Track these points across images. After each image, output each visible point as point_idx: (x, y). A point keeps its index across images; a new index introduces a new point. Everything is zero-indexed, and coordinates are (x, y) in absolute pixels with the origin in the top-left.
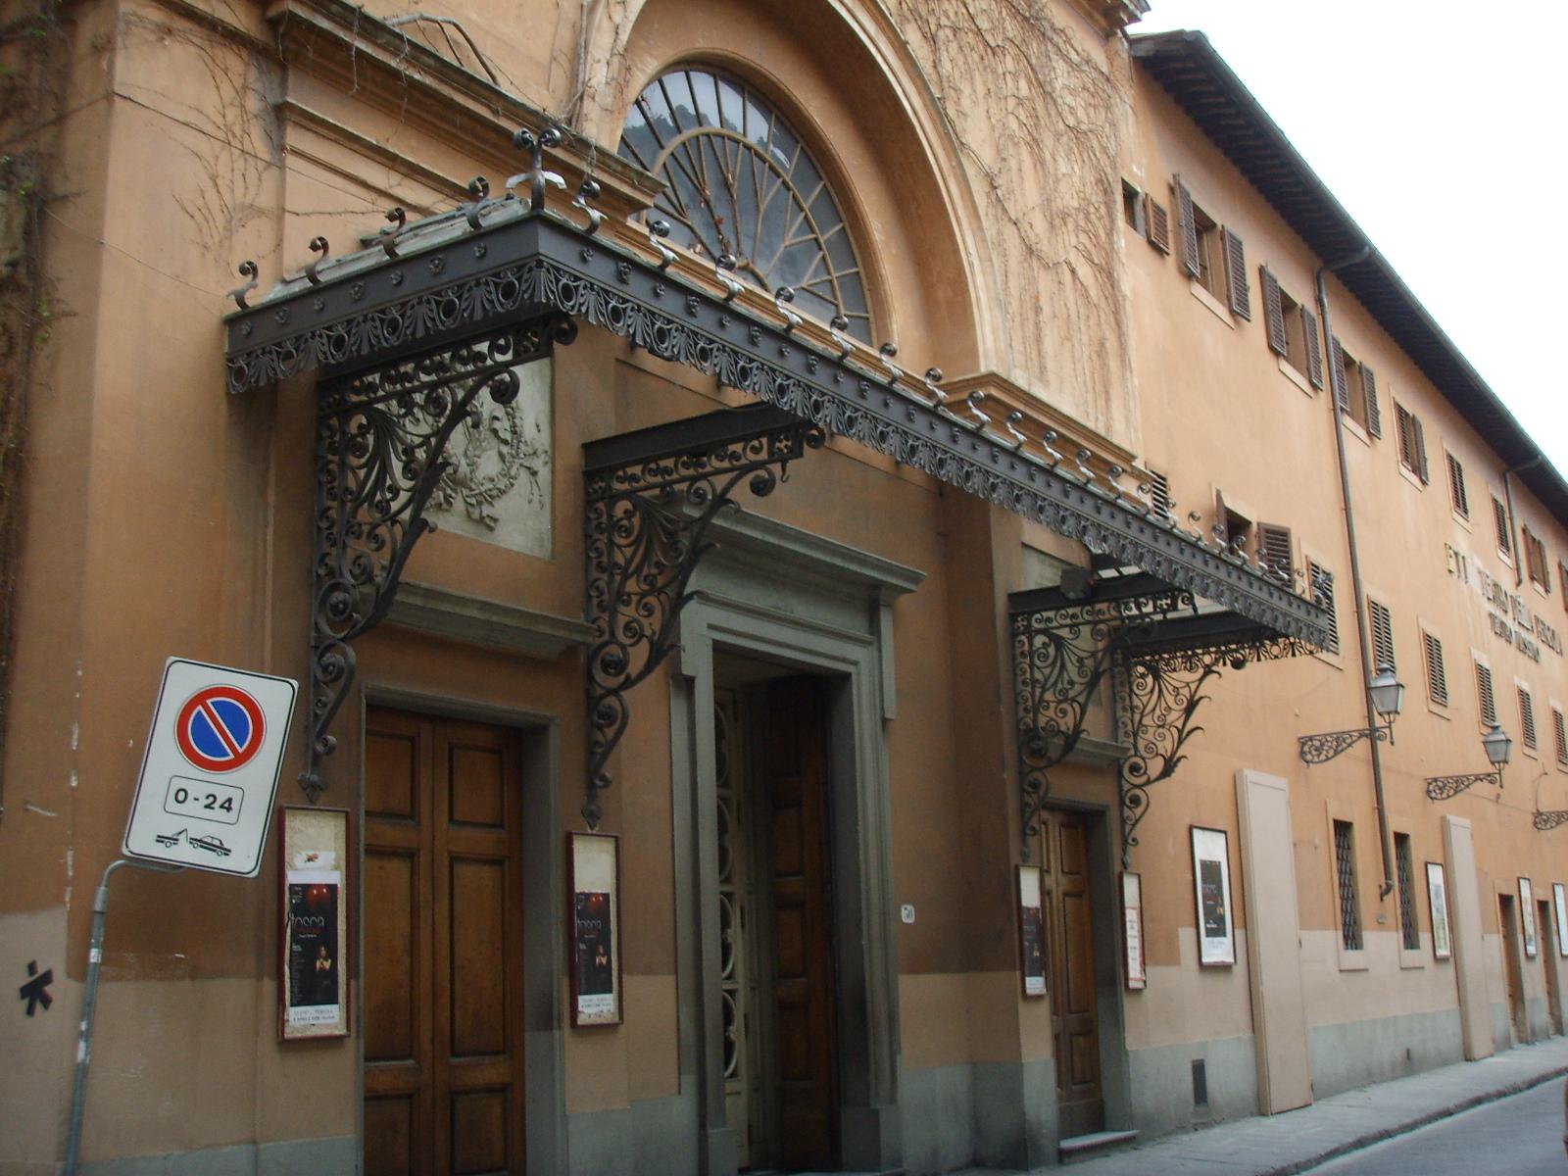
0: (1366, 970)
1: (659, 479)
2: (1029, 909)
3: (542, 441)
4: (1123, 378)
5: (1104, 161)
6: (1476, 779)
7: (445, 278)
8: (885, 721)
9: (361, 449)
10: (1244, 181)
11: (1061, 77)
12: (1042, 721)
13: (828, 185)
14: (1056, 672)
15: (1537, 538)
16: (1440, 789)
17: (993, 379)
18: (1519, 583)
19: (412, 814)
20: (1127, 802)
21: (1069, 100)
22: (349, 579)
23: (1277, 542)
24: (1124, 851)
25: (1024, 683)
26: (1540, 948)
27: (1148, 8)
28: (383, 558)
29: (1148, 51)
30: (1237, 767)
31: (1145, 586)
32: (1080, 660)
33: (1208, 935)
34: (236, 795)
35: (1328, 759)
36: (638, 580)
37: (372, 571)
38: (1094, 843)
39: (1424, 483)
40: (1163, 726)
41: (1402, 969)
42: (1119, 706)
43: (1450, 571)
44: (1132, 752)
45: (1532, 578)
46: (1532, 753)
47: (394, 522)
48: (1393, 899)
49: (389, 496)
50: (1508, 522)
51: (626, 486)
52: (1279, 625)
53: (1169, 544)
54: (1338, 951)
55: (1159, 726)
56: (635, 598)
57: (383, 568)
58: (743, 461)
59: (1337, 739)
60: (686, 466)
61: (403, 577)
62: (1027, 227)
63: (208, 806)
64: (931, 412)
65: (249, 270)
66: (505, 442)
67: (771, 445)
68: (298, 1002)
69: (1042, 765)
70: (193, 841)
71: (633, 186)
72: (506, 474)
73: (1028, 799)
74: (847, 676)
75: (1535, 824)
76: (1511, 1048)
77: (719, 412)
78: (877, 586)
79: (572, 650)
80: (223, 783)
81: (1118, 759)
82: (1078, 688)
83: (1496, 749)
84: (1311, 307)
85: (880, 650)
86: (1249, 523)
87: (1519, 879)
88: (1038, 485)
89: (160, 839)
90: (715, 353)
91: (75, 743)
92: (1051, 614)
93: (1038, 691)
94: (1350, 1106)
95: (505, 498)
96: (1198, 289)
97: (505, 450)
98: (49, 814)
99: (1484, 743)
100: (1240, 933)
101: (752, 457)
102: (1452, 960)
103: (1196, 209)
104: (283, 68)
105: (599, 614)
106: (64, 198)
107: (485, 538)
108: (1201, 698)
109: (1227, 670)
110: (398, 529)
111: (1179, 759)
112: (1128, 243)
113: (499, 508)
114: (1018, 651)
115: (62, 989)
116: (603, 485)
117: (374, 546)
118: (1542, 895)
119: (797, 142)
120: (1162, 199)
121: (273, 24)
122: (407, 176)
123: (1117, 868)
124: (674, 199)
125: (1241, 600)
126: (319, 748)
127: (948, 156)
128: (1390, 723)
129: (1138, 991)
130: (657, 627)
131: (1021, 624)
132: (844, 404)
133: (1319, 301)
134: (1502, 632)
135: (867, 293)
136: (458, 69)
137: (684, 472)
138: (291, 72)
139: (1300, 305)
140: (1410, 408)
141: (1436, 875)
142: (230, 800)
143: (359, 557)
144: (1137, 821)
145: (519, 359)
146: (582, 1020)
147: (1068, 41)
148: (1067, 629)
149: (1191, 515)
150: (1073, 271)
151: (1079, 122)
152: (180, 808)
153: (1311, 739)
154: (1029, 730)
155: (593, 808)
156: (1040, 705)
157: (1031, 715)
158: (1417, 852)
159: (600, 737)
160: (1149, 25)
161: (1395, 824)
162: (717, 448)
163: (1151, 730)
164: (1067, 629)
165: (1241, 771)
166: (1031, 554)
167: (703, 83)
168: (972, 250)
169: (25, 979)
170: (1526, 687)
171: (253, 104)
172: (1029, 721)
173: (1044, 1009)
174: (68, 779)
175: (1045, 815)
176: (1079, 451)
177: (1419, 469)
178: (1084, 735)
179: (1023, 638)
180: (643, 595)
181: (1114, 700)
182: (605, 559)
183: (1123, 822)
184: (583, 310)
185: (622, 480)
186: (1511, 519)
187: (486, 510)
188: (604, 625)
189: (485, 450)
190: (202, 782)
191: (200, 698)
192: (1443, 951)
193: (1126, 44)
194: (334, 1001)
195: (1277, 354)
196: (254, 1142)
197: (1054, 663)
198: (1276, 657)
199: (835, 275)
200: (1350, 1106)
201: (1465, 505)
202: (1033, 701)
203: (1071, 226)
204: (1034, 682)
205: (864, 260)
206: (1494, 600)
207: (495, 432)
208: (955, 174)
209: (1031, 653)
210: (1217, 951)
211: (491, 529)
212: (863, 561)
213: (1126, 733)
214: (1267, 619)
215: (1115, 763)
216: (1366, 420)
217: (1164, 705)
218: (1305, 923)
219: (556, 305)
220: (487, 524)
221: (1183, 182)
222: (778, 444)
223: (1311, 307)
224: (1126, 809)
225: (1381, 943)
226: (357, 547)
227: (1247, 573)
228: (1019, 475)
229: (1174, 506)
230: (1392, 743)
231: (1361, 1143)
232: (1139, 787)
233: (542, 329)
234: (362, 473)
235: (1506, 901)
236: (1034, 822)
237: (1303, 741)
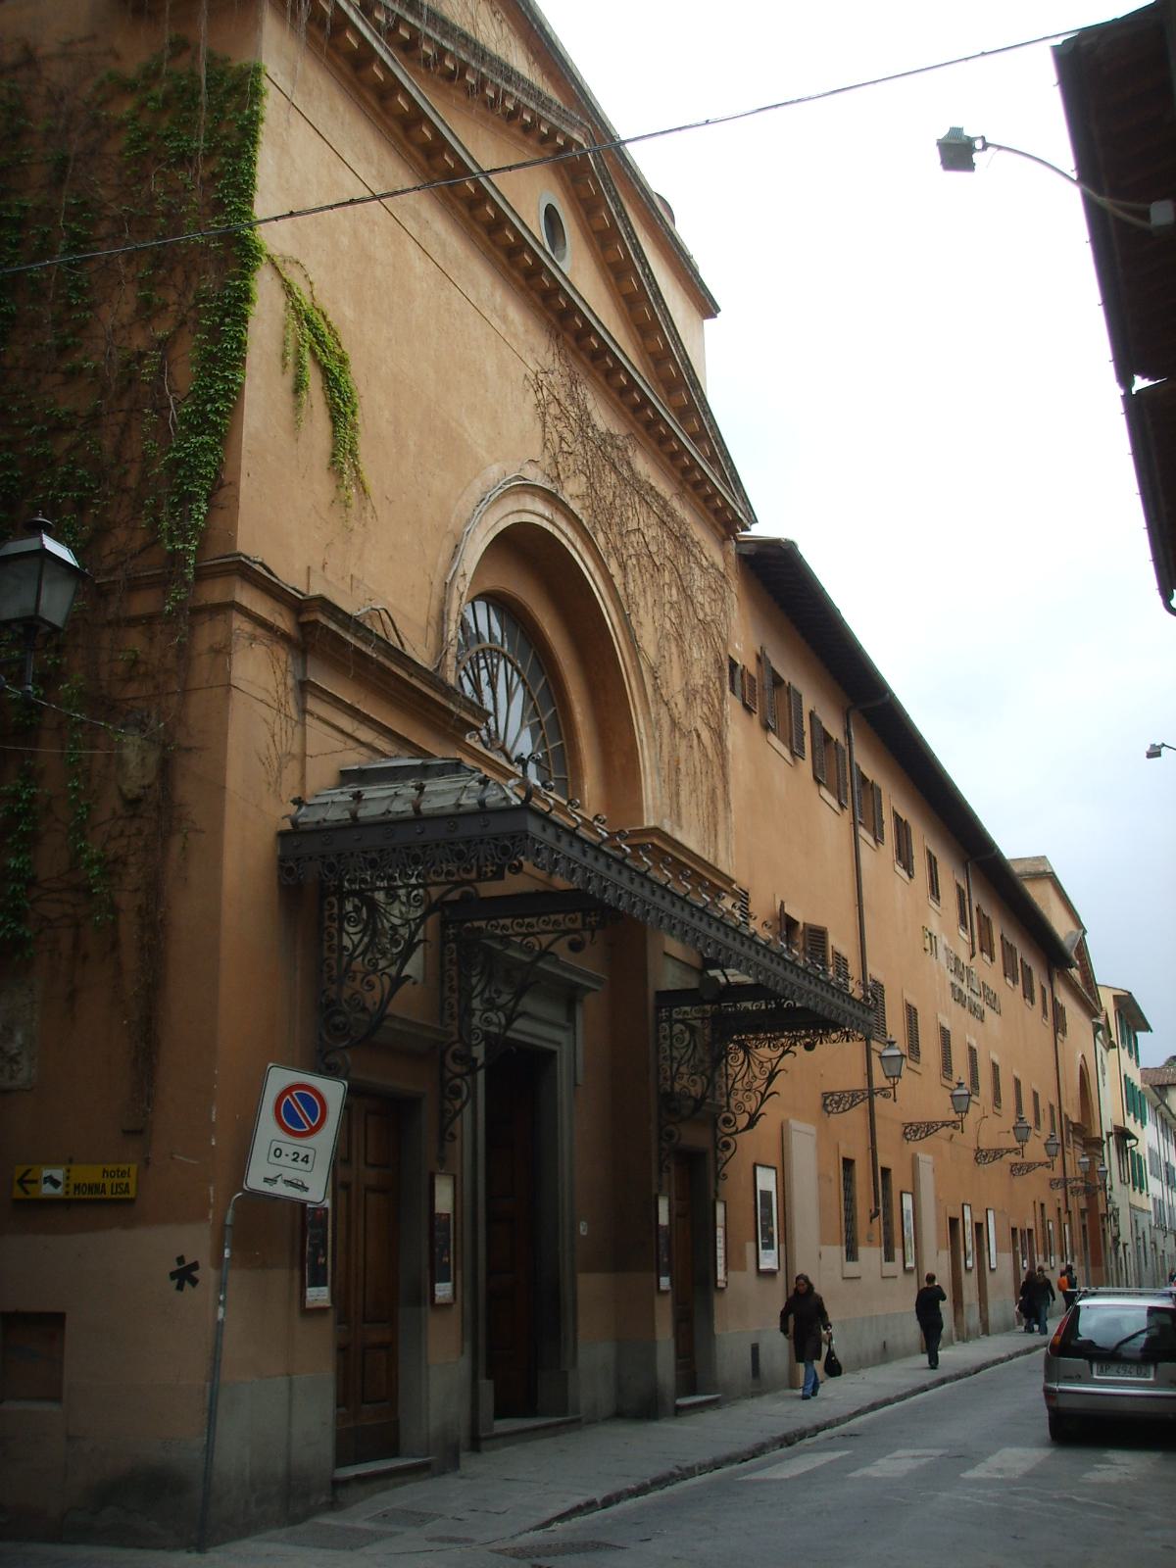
0: (859, 1278)
2: (663, 1227)
4: (726, 818)
5: (720, 644)
6: (943, 1126)
11: (699, 581)
12: (347, 993)
14: (690, 1052)
15: (987, 915)
16: (914, 1131)
17: (656, 831)
18: (973, 956)
20: (720, 1146)
21: (700, 598)
23: (817, 936)
26: (976, 1263)
29: (750, 551)
30: (791, 1123)
33: (763, 1248)
34: (311, 1153)
35: (845, 1111)
38: (698, 1175)
39: (911, 877)
40: (749, 1090)
41: (883, 1277)
43: (925, 949)
45: (982, 950)
46: (997, 1110)
48: (878, 1222)
50: (967, 903)
54: (842, 1262)
55: (747, 1090)
58: (562, 927)
59: (853, 1095)
62: (674, 705)
63: (294, 1160)
68: (312, 1285)
70: (286, 1181)
71: (474, 716)
73: (664, 1144)
74: (554, 1053)
75: (976, 1159)
76: (952, 1344)
77: (545, 893)
78: (577, 987)
80: (303, 1145)
83: (961, 1104)
84: (842, 741)
85: (575, 1034)
86: (798, 923)
87: (963, 1205)
89: (266, 1180)
91: (214, 1117)
92: (687, 1009)
93: (675, 1065)
94: (852, 1383)
98: (192, 1162)
99: (951, 1096)
100: (782, 1246)
101: (570, 925)
102: (915, 1271)
106: (189, 750)
108: (780, 1071)
109: (799, 1048)
111: (760, 1115)
112: (732, 706)
115: (207, 1274)
118: (978, 1219)
119: (531, 647)
120: (752, 667)
121: (302, 626)
122: (380, 734)
123: (713, 1195)
127: (631, 659)
128: (894, 1084)
129: (722, 1289)
131: (664, 1014)
133: (847, 734)
134: (960, 998)
135: (567, 761)
136: (396, 649)
138: (309, 657)
139: (787, 683)
140: (904, 815)
141: (908, 1201)
142: (307, 1156)
144: (727, 1161)
146: (438, 1300)
147: (701, 552)
148: (700, 1021)
150: (699, 736)
151: (706, 615)
152: (276, 1160)
153: (832, 1094)
157: (669, 1083)
158: (898, 1181)
159: (447, 1105)
161: (882, 1161)
163: (741, 1093)
164: (700, 1021)
165: (788, 1121)
166: (669, 963)
168: (643, 731)
169: (175, 1267)
170: (974, 1044)
171: (290, 682)
173: (668, 1300)
174: (210, 1140)
177: (908, 867)
179: (333, 900)
183: (717, 1161)
186: (970, 900)
190: (290, 1145)
191: (288, 1090)
192: (910, 1264)
193: (734, 544)
194: (325, 1285)
196: (288, 1375)
197: (688, 1045)
198: (834, 1042)
199: (550, 747)
200: (852, 1383)
201: (938, 892)
202: (671, 1073)
203: (699, 701)
204: (673, 1059)
206: (955, 971)
208: (635, 672)
210: (769, 1260)
213: (665, 1078)
216: (874, 829)
217: (751, 1075)
218: (823, 1242)
221: (768, 654)
223: (842, 741)
224: (718, 1152)
225: (870, 1255)
229: (755, 918)
230: (963, 1132)
231: (874, 1407)
232: (730, 1135)
235: (953, 1222)
237: (826, 1095)
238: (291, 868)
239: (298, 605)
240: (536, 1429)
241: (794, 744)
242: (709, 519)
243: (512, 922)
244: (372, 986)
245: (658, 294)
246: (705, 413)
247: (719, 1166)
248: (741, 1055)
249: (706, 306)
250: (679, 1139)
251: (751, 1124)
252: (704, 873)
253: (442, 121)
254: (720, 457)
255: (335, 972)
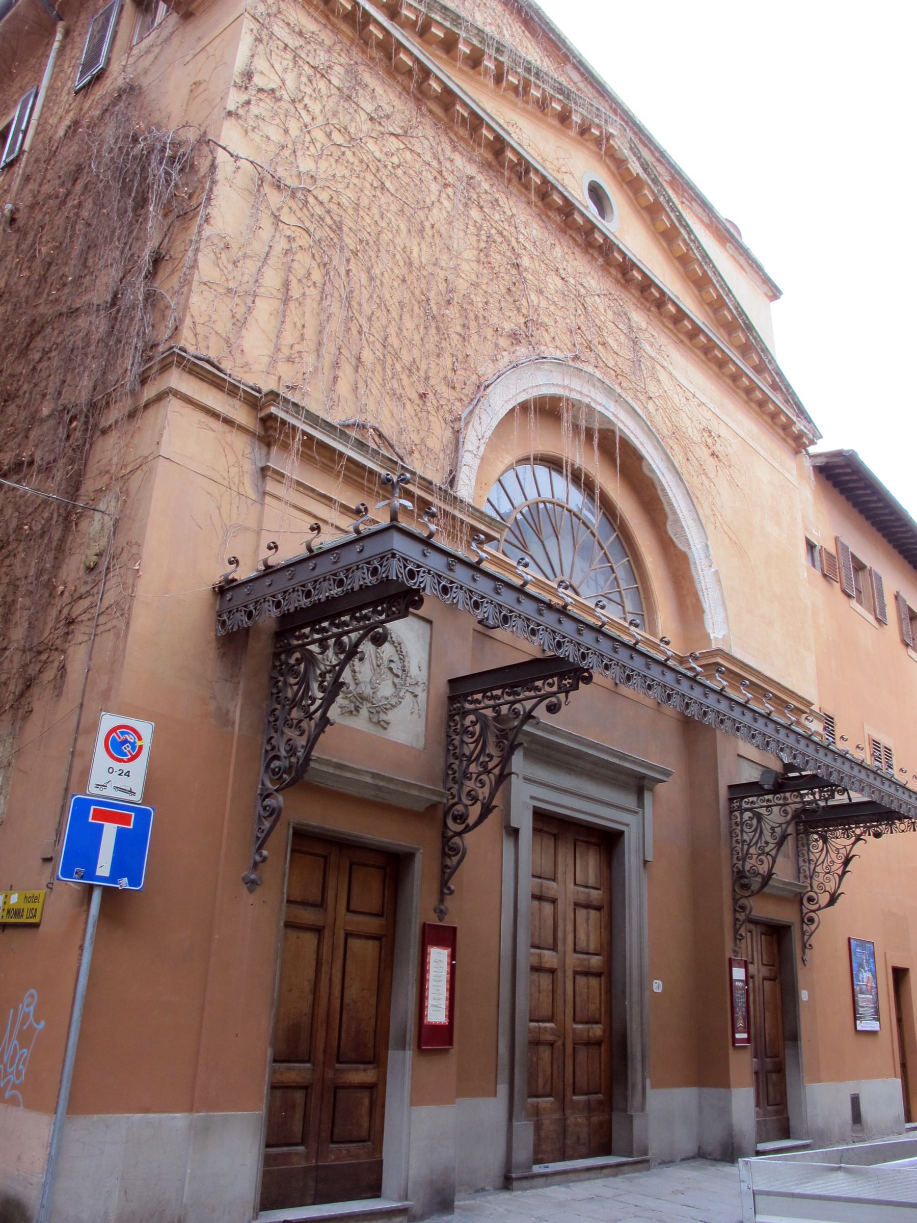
1: (492, 702)
3: (422, 677)
7: (339, 565)
8: (645, 862)
9: (296, 674)
10: (885, 541)
12: (747, 867)
13: (620, 536)
14: (757, 835)
17: (719, 652)
19: (320, 905)
20: (806, 921)
22: (283, 753)
24: (804, 953)
25: (737, 841)
27: (821, 437)
28: (302, 741)
31: (814, 782)
32: (773, 828)
36: (477, 765)
37: (296, 749)
40: (828, 873)
42: (801, 859)
44: (809, 889)
47: (311, 719)
49: (487, 759)
51: (472, 706)
52: (903, 810)
53: (826, 755)
55: (827, 873)
56: (474, 776)
57: (303, 747)
58: (543, 692)
60: (509, 694)
61: (315, 754)
64: (693, 679)
65: (234, 561)
66: (397, 676)
67: (560, 682)
69: (747, 895)
72: (397, 695)
73: (738, 916)
74: (621, 833)
78: (643, 777)
79: (434, 806)
81: (801, 893)
82: (771, 846)
88: (736, 713)
90: (454, 590)
95: (395, 710)
96: (854, 603)
97: (397, 680)
101: (548, 689)
103: (853, 557)
104: (269, 445)
105: (452, 785)
107: (381, 733)
108: (854, 856)
109: (871, 839)
110: (313, 723)
111: (840, 894)
113: (390, 716)
114: (734, 821)
116: (458, 705)
117: (298, 733)
124: (519, 536)
125: (877, 792)
126: (258, 858)
130: (487, 795)
132: (602, 656)
137: (507, 698)
143: (290, 740)
144: (812, 933)
145: (390, 619)
149: (857, 747)
154: (739, 872)
155: (442, 907)
156: (746, 856)
159: (448, 862)
160: (821, 447)
162: (527, 684)
167: (542, 472)
171: (248, 466)
172: (740, 866)
175: (752, 927)
176: (786, 705)
178: (774, 876)
180: (479, 774)
181: (798, 855)
182: (458, 751)
184: (455, 601)
185: (471, 702)
187: (383, 716)
188: (454, 791)
189: (384, 680)
195: (907, 645)
197: (755, 830)
205: (641, 580)
207: (391, 669)
209: (742, 823)
211: (385, 729)
212: (624, 757)
213: (805, 876)
214: (894, 806)
215: (799, 899)
217: (829, 860)
219: (403, 582)
220: (383, 725)
222: (564, 682)
224: (805, 925)
226: (291, 733)
227: (832, 751)
228: (723, 706)
232: (814, 911)
233: (403, 599)
234: (295, 688)
236: (742, 931)
238: (224, 621)
239: (255, 401)
240: (589, 1169)
241: (878, 612)
242: (778, 434)
243: (503, 693)
244: (762, 862)
245: (706, 256)
246: (763, 351)
247: (806, 937)
248: (821, 843)
249: (774, 293)
250: (751, 911)
251: (833, 900)
252: (743, 673)
253: (449, 77)
254: (780, 385)
255: (740, 855)
